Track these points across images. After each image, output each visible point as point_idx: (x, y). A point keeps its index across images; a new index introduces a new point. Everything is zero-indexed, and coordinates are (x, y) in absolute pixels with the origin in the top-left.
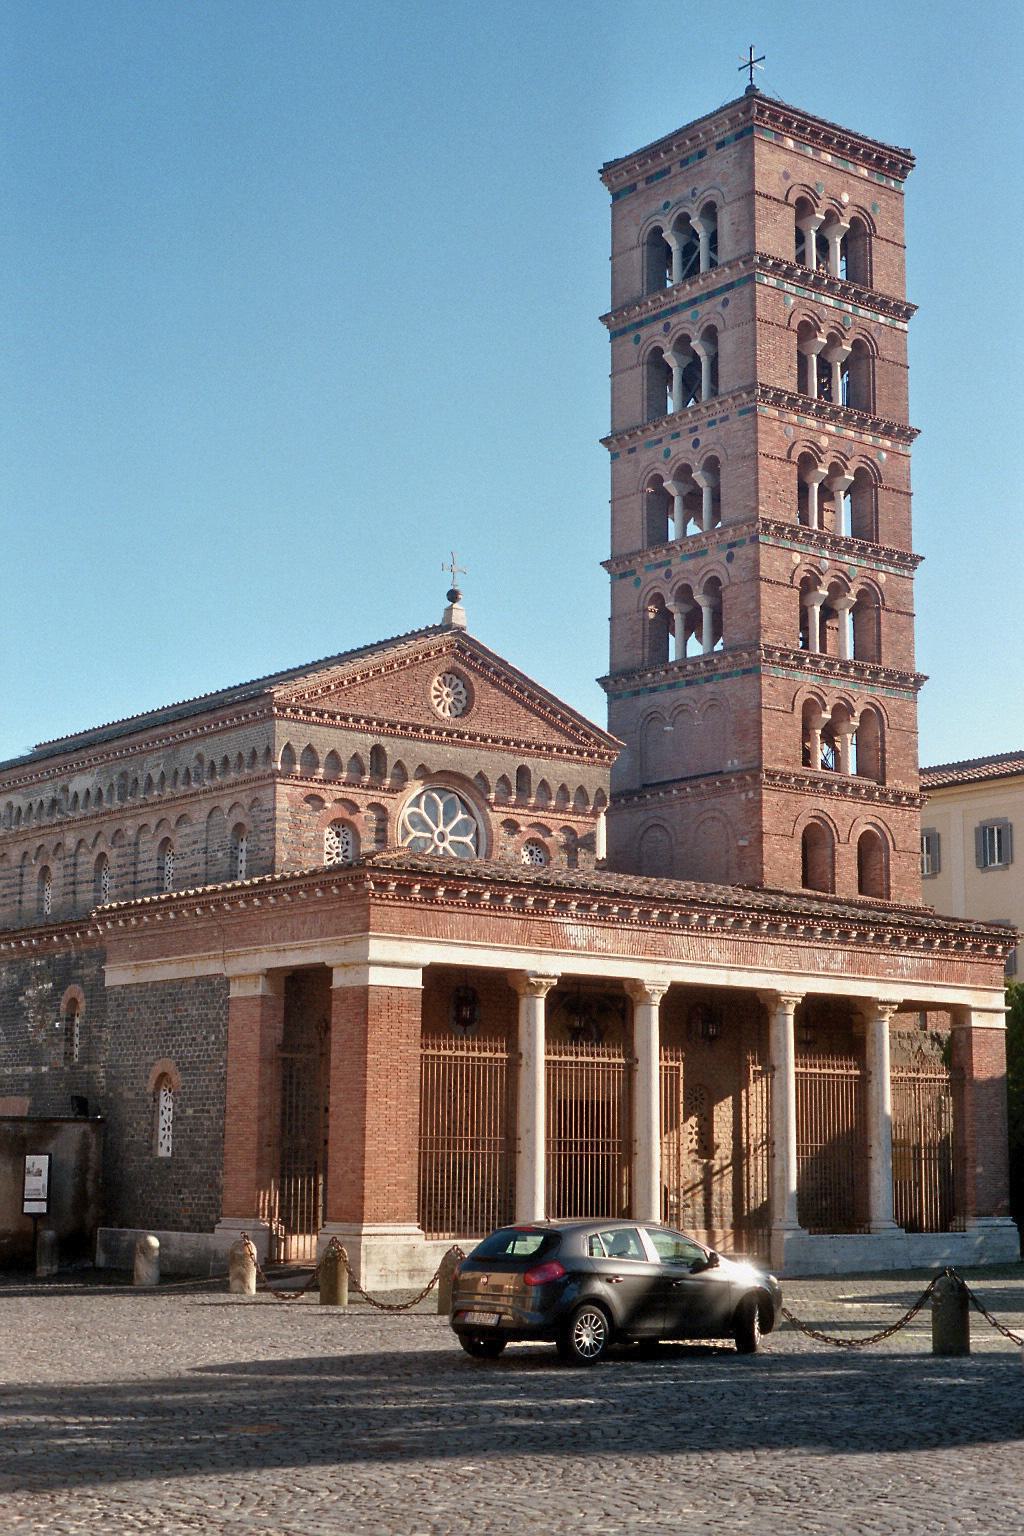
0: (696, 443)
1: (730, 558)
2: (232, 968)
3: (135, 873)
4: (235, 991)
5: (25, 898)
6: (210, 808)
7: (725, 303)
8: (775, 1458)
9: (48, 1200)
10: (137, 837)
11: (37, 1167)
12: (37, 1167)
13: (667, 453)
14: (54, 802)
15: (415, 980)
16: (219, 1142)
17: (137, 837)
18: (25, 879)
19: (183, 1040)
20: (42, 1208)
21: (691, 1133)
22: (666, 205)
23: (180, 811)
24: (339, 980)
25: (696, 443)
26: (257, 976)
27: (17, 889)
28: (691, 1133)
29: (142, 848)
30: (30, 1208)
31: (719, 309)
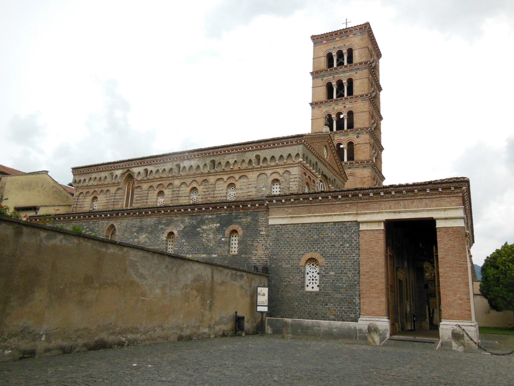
0: (345, 107)
1: (358, 137)
2: (360, 219)
3: (214, 194)
4: (362, 227)
5: (148, 201)
6: (168, 183)
7: (356, 73)
8: (79, 355)
9: (269, 306)
10: (216, 183)
11: (262, 292)
12: (262, 292)
13: (334, 109)
14: (171, 169)
15: (382, 227)
16: (355, 285)
17: (216, 183)
18: (149, 195)
19: (326, 246)
20: (265, 309)
21: (310, 280)
22: (334, 48)
23: (107, 189)
24: (439, 224)
25: (345, 107)
26: (380, 222)
27: (146, 198)
28: (310, 280)
29: (217, 186)
30: (260, 309)
31: (354, 74)
